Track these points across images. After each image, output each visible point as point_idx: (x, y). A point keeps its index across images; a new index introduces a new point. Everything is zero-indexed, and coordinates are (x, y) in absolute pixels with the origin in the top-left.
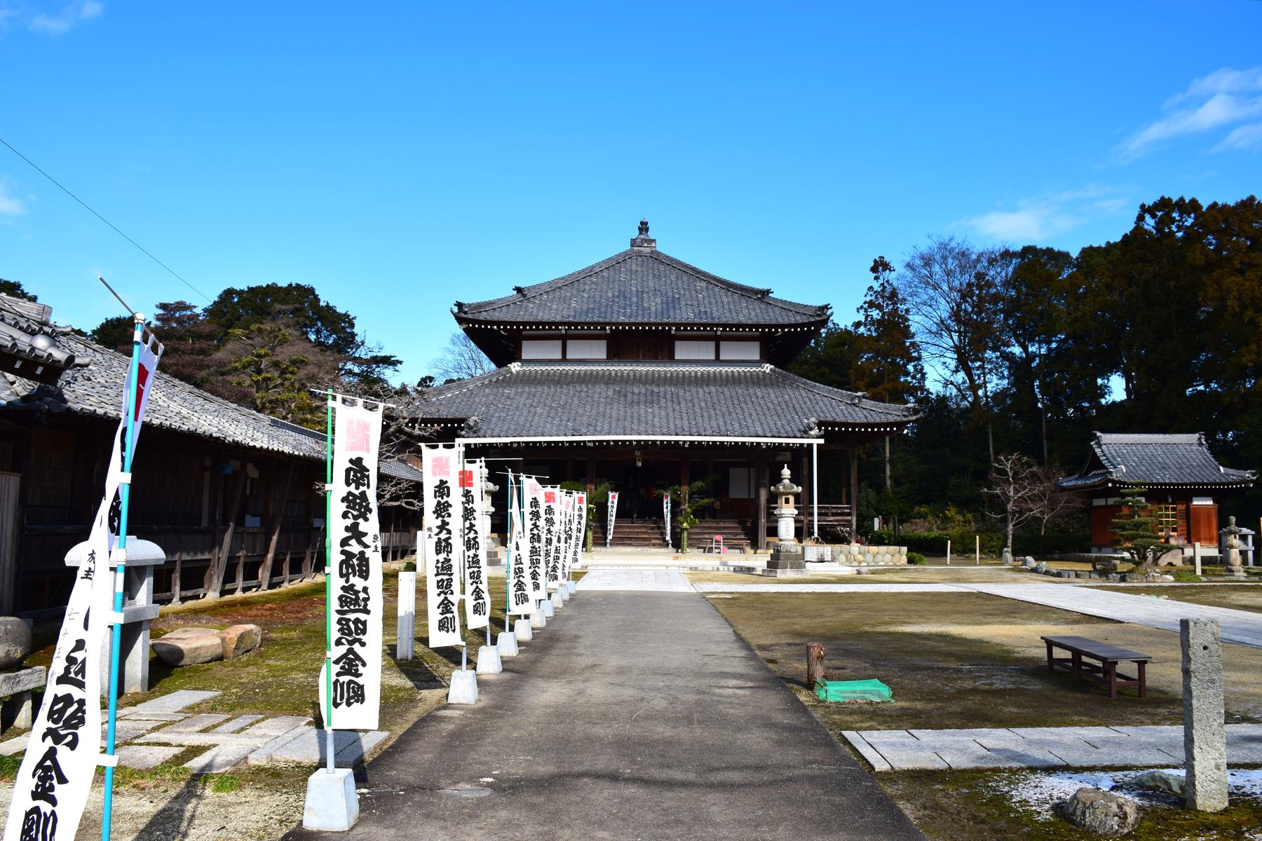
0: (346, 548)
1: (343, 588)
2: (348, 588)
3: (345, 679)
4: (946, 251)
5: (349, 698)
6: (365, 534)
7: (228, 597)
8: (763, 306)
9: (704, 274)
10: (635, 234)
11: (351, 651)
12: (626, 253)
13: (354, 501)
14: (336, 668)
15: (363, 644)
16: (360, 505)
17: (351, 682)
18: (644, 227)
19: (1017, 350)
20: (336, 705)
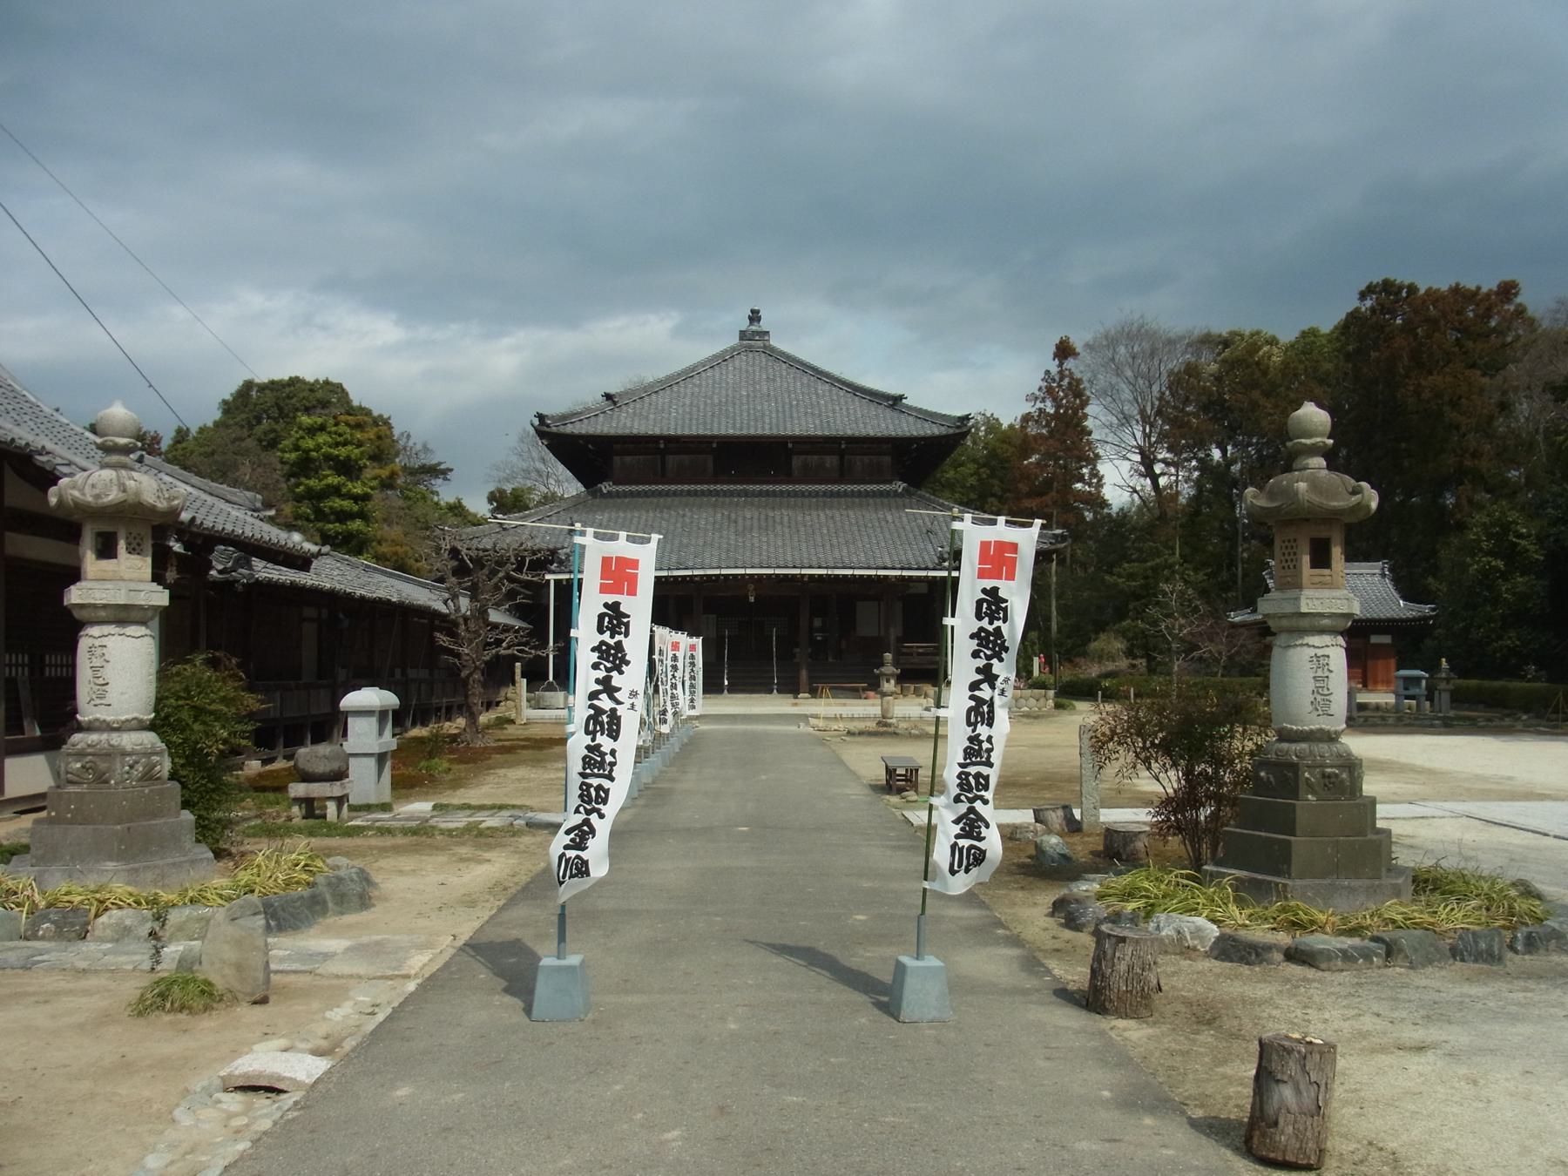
0: (977, 693)
1: (588, 748)
2: (974, 739)
3: (571, 854)
4: (1133, 334)
5: (969, 864)
6: (619, 689)
7: (269, 767)
8: (896, 414)
9: (827, 375)
10: (744, 324)
11: (972, 810)
12: (733, 349)
13: (607, 651)
14: (567, 840)
15: (602, 816)
16: (994, 643)
17: (971, 847)
18: (755, 317)
19: (1216, 454)
20: (953, 872)
